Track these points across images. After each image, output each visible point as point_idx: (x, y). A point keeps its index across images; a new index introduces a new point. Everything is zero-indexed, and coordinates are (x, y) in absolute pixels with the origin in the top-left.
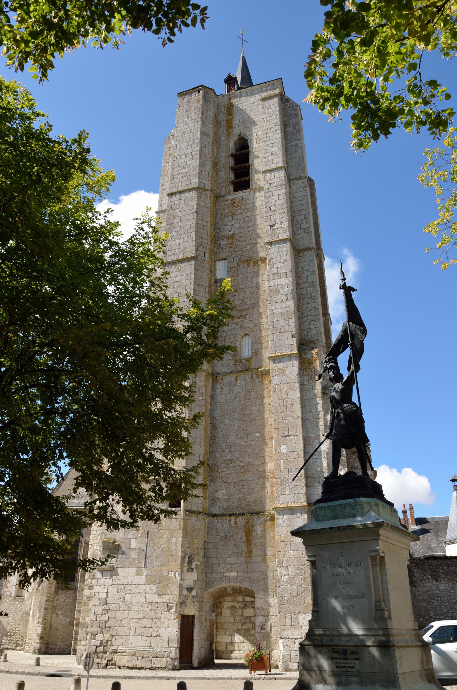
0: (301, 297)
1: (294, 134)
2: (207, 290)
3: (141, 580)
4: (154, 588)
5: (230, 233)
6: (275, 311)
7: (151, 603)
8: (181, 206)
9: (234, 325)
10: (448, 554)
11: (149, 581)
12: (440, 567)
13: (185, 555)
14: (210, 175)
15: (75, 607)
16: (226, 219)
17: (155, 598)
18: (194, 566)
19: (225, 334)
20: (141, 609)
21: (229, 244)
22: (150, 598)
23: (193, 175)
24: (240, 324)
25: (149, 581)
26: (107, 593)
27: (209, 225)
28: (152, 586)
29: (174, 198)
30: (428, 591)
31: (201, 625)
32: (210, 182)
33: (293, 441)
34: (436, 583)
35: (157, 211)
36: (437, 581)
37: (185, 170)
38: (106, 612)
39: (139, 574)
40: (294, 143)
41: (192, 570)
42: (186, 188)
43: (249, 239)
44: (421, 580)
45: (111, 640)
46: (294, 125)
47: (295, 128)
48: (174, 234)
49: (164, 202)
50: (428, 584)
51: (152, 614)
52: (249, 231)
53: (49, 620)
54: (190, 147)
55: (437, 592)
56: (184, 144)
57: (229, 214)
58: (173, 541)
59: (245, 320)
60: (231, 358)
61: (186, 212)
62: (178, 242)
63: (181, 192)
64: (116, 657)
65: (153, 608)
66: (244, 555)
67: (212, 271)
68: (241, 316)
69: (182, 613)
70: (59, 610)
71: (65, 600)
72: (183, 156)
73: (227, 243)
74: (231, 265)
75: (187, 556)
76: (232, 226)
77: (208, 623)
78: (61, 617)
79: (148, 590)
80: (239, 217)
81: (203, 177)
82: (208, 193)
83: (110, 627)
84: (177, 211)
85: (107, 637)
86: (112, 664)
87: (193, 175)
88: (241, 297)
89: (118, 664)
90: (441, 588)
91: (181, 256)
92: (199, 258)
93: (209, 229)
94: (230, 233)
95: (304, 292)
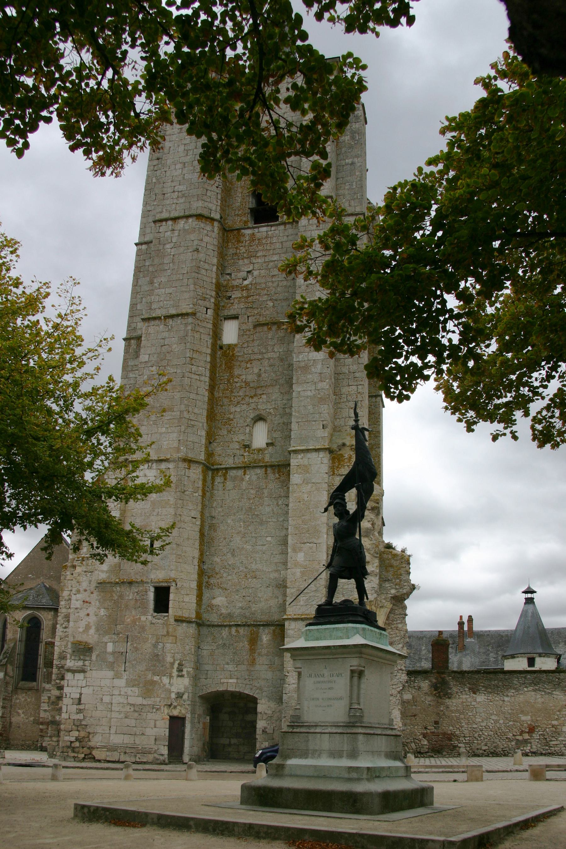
0: (341, 376)
1: (351, 147)
2: (209, 359)
3: (121, 683)
4: (137, 691)
5: (246, 283)
6: (302, 394)
7: (133, 705)
8: (174, 240)
9: (244, 407)
10: (506, 669)
11: (131, 683)
12: (481, 681)
13: (174, 660)
14: (219, 197)
15: (40, 706)
16: (241, 262)
17: (140, 701)
18: (184, 673)
19: (232, 417)
20: (122, 710)
21: (243, 297)
22: (132, 700)
23: (193, 196)
24: (253, 406)
25: (131, 683)
26: (81, 694)
27: (215, 268)
28: (136, 689)
29: (164, 227)
30: (463, 702)
31: (192, 728)
32: (219, 208)
33: (314, 549)
34: (474, 695)
35: (137, 241)
36: (474, 693)
37: (181, 188)
38: (80, 711)
39: (117, 676)
40: (349, 161)
41: (182, 676)
42: (182, 214)
43: (272, 292)
44: (457, 693)
45: (88, 737)
46: (353, 133)
47: (353, 138)
48: (163, 279)
49: (148, 230)
50: (464, 696)
51: (136, 714)
52: (273, 282)
53: (8, 719)
54: (190, 153)
55: (473, 703)
56: (182, 148)
57: (245, 255)
58: (159, 647)
59: (261, 400)
60: (238, 447)
61: (182, 249)
62: (168, 291)
63: (175, 219)
64: (94, 753)
65: (137, 709)
66: (246, 663)
67: (217, 334)
68: (255, 395)
69: (171, 714)
70: (19, 709)
71: (26, 700)
72: (179, 166)
73: (240, 295)
74: (244, 327)
75: (177, 662)
76: (249, 272)
77: (201, 725)
78: (22, 715)
79: (130, 693)
80: (259, 260)
81: (208, 200)
82: (216, 224)
83: (86, 725)
84: (168, 246)
85: (83, 734)
86: (90, 758)
87: (193, 196)
88: (256, 371)
89: (97, 757)
90: (478, 700)
91: (173, 312)
92: (198, 315)
93: (214, 276)
94: (246, 283)
95: (345, 370)
